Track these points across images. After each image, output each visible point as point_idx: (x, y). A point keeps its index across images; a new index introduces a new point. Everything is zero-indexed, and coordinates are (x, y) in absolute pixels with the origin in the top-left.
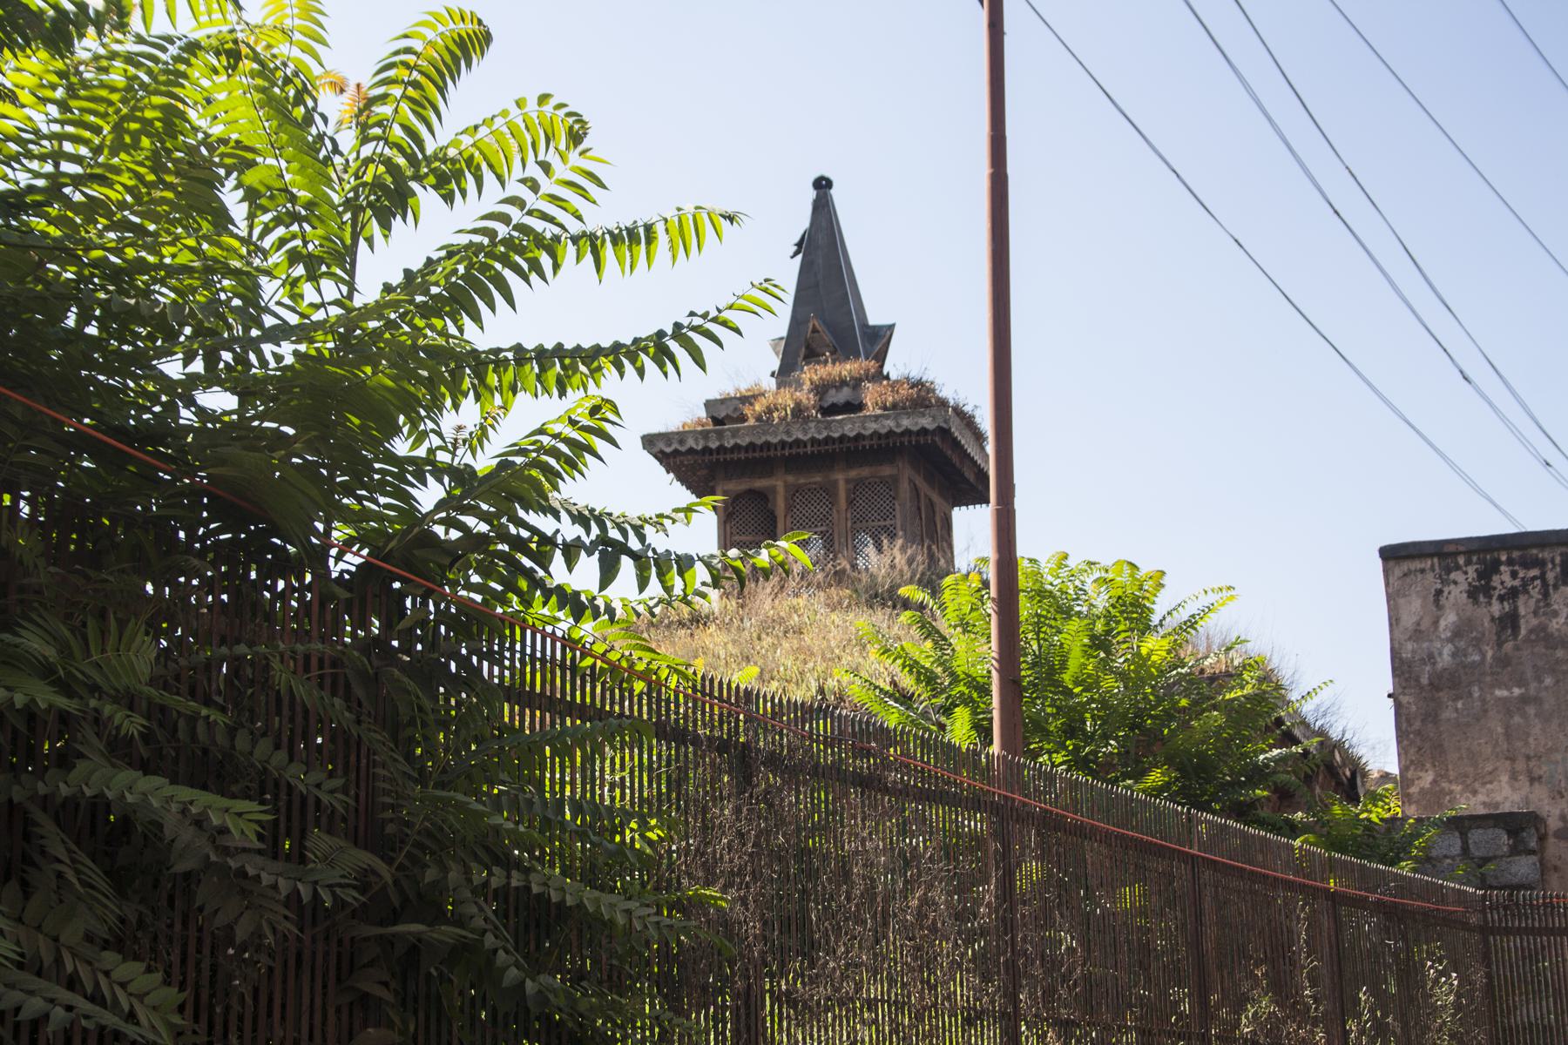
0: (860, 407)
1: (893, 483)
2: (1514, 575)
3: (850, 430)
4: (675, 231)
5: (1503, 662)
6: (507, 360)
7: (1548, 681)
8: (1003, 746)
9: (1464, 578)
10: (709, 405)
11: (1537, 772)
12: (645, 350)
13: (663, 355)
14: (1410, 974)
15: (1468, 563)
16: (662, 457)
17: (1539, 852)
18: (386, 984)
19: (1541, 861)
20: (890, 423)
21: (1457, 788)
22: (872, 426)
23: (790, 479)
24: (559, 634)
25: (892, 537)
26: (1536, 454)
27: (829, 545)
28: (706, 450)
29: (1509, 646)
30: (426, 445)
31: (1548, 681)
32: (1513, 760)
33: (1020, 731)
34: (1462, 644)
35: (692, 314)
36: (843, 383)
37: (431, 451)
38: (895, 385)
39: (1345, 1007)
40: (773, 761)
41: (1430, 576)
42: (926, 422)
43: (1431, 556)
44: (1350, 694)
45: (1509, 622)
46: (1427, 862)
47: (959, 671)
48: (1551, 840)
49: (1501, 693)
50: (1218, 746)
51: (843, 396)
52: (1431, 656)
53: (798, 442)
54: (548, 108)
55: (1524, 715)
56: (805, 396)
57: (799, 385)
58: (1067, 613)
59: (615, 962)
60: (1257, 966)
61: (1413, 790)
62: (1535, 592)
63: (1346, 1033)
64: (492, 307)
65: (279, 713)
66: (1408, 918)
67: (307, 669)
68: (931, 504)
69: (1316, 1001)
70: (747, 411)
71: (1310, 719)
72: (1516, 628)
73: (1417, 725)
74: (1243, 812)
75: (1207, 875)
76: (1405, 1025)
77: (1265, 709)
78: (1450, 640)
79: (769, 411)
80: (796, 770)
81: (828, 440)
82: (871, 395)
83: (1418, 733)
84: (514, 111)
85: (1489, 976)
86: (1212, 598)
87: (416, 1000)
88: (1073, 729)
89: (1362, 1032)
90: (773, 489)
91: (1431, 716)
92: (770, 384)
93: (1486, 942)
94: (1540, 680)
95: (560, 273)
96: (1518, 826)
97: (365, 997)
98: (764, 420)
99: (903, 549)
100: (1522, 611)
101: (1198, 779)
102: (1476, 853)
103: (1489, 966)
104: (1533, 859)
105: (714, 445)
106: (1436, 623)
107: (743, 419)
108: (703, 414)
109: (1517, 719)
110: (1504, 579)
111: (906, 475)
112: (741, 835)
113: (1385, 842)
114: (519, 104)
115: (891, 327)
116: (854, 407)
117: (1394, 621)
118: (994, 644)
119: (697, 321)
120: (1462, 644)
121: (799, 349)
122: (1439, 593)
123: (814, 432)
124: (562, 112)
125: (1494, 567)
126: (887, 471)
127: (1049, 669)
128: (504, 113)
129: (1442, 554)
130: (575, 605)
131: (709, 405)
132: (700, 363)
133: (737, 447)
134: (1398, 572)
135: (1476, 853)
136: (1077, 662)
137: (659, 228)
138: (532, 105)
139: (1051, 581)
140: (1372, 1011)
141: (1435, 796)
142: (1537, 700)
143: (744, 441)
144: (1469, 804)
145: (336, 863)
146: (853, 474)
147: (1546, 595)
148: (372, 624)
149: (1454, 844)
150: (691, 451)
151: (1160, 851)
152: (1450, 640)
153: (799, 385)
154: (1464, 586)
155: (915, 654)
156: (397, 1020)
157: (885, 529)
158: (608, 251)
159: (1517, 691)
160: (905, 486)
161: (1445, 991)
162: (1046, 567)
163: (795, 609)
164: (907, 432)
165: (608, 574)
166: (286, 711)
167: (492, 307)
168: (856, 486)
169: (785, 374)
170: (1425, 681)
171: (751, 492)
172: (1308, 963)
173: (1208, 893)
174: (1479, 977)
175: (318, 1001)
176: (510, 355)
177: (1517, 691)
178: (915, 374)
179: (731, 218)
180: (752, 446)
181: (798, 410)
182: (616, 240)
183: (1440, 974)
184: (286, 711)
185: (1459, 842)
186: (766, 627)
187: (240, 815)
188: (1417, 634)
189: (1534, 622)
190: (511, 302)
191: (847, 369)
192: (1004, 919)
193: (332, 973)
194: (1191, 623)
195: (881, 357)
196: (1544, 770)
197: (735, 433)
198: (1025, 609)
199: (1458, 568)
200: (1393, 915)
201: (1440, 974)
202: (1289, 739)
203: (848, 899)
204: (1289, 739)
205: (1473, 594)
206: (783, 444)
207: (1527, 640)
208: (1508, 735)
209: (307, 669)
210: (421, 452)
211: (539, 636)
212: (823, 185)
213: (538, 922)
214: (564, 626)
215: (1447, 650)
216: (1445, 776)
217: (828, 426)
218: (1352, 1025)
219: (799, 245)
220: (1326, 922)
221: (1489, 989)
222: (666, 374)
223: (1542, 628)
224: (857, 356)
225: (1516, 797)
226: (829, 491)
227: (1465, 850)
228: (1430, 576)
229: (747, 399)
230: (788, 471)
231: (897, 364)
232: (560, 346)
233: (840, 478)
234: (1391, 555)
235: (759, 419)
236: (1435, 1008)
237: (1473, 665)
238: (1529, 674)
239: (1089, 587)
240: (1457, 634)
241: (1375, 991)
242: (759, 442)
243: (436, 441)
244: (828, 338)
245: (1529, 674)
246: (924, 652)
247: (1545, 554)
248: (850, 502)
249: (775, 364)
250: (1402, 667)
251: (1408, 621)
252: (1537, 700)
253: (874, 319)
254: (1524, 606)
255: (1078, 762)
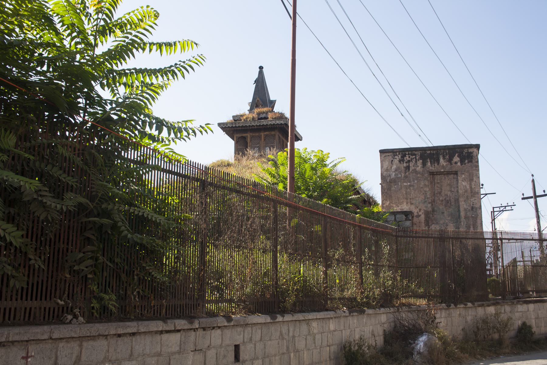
0: (267, 118)
1: (275, 135)
2: (409, 157)
3: (265, 123)
5: (406, 177)
6: (133, 72)
7: (416, 182)
8: (290, 190)
10: (233, 117)
11: (412, 202)
13: (174, 74)
15: (399, 154)
16: (222, 128)
18: (94, 235)
20: (274, 122)
21: (394, 205)
22: (270, 123)
23: (251, 134)
24: (152, 148)
25: (273, 148)
26: (418, 134)
27: (260, 151)
28: (232, 127)
29: (407, 173)
31: (416, 182)
32: (407, 199)
33: (294, 187)
34: (397, 173)
36: (264, 113)
37: (117, 99)
39: (362, 252)
40: (211, 184)
41: (390, 157)
42: (282, 122)
43: (391, 152)
44: (372, 185)
46: (386, 221)
47: (281, 174)
50: (343, 195)
52: (390, 175)
53: (253, 126)
54: (149, 9)
55: (410, 189)
56: (255, 115)
58: (305, 161)
62: (414, 161)
63: (361, 259)
64: (129, 57)
65: (65, 162)
66: (380, 234)
67: (75, 151)
68: (283, 141)
70: (242, 118)
71: (366, 191)
72: (409, 169)
73: (386, 191)
74: (346, 209)
76: (376, 258)
77: (353, 186)
78: (394, 172)
79: (247, 118)
81: (260, 125)
82: (270, 115)
84: (140, 9)
85: (397, 247)
86: (340, 160)
87: (104, 240)
88: (307, 189)
89: (365, 259)
90: (247, 136)
91: (389, 189)
93: (397, 239)
94: (414, 181)
97: (88, 239)
98: (246, 120)
101: (336, 201)
103: (397, 244)
105: (234, 126)
106: (391, 168)
107: (241, 120)
109: (408, 190)
110: (407, 158)
111: (277, 134)
114: (142, 8)
115: (275, 101)
116: (266, 118)
117: (382, 167)
118: (289, 168)
120: (397, 173)
121: (254, 105)
122: (392, 161)
123: (256, 123)
124: (153, 10)
125: (405, 155)
126: (273, 133)
127: (302, 175)
128: (137, 10)
130: (152, 138)
131: (233, 117)
134: (383, 156)
136: (308, 173)
138: (145, 8)
140: (368, 254)
141: (389, 207)
142: (413, 186)
144: (397, 209)
145: (71, 200)
147: (416, 162)
148: (95, 140)
149: (393, 218)
150: (229, 127)
151: (317, 214)
152: (394, 172)
156: (97, 245)
158: (164, 48)
159: (409, 184)
160: (277, 136)
161: (386, 250)
162: (301, 151)
163: (251, 163)
164: (278, 124)
165: (160, 130)
167: (129, 57)
168: (266, 136)
169: (251, 110)
170: (388, 181)
171: (242, 137)
172: (353, 242)
174: (395, 247)
175: (74, 239)
176: (134, 71)
177: (409, 184)
178: (280, 111)
181: (253, 118)
183: (385, 246)
185: (394, 218)
186: (244, 167)
187: (31, 183)
188: (387, 170)
189: (413, 168)
190: (134, 56)
191: (265, 109)
193: (79, 231)
195: (273, 107)
196: (414, 202)
197: (239, 123)
198: (297, 160)
199: (397, 155)
200: (374, 232)
201: (385, 246)
203: (232, 220)
204: (358, 193)
205: (400, 161)
206: (250, 126)
207: (411, 172)
208: (406, 194)
210: (115, 99)
211: (145, 148)
212: (261, 68)
214: (153, 146)
215: (394, 174)
216: (392, 203)
217: (260, 122)
218: (363, 257)
219: (255, 81)
220: (358, 233)
221: (397, 250)
223: (415, 169)
224: (267, 107)
225: (407, 208)
226: (260, 137)
227: (395, 219)
228: (390, 157)
229: (242, 116)
230: (251, 132)
231: (276, 109)
232: (146, 69)
233: (262, 134)
234: (382, 152)
236: (384, 254)
239: (312, 157)
240: (396, 170)
241: (370, 249)
242: (244, 125)
243: (118, 96)
244: (261, 103)
247: (417, 153)
248: (264, 140)
249: (249, 108)
250: (383, 177)
251: (385, 167)
254: (411, 164)
255: (310, 197)
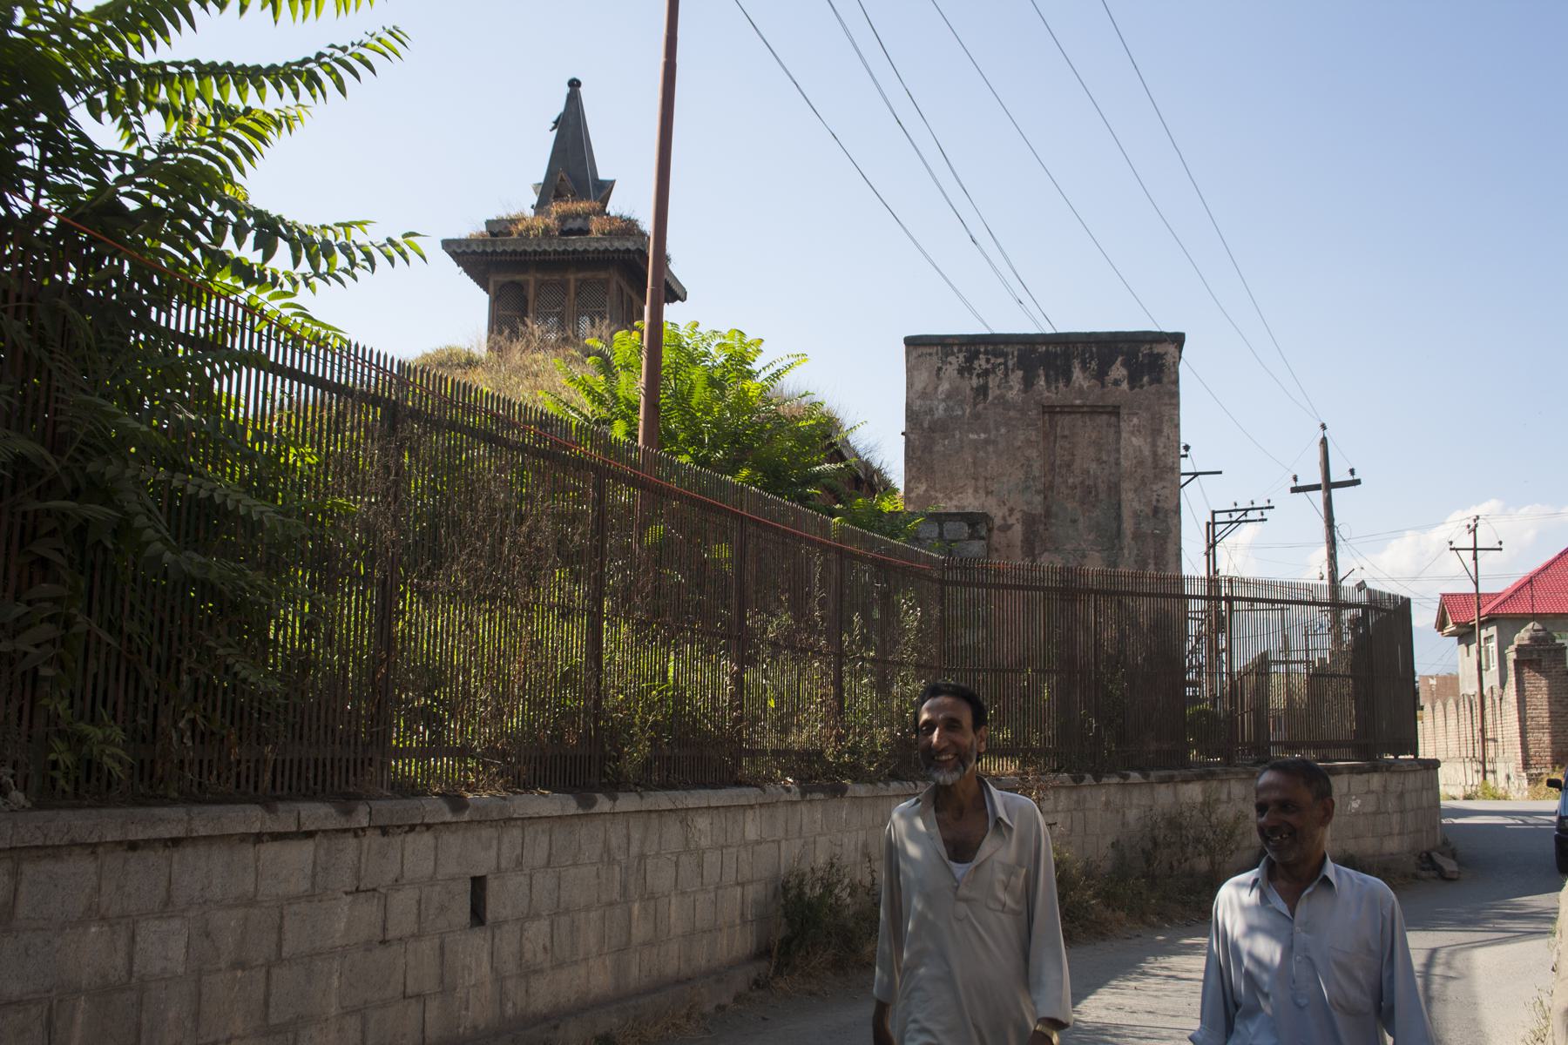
0: (588, 232)
2: (988, 361)
3: (580, 247)
5: (976, 416)
6: (189, 73)
8: (645, 442)
9: (957, 360)
10: (488, 223)
13: (313, 81)
14: (890, 609)
17: (988, 538)
18: (60, 551)
19: (988, 545)
20: (606, 244)
21: (940, 496)
22: (595, 245)
23: (539, 276)
24: (241, 301)
25: (602, 318)
26: (1014, 295)
28: (484, 253)
29: (980, 407)
30: (135, 145)
31: (1003, 431)
32: (976, 479)
35: (332, 46)
36: (578, 215)
37: (140, 150)
38: (611, 219)
39: (843, 624)
40: (415, 414)
42: (630, 245)
44: (879, 434)
45: (982, 391)
46: (915, 539)
47: (620, 394)
51: (577, 224)
52: (931, 410)
53: (545, 252)
56: (552, 221)
57: (549, 214)
61: (913, 495)
62: (1000, 373)
63: (841, 643)
66: (895, 573)
69: (823, 620)
70: (513, 229)
72: (986, 395)
73: (919, 453)
74: (804, 499)
75: (751, 529)
76: (883, 641)
77: (825, 436)
79: (528, 229)
82: (595, 224)
83: (919, 459)
85: (942, 611)
86: (792, 360)
88: (695, 440)
89: (852, 642)
90: (527, 282)
91: (928, 448)
92: (530, 213)
96: (975, 521)
98: (524, 235)
101: (774, 477)
102: (947, 536)
105: (489, 249)
106: (936, 388)
107: (510, 234)
108: (484, 229)
109: (981, 454)
110: (981, 363)
111: (615, 279)
113: (893, 524)
115: (613, 182)
116: (584, 232)
118: (643, 380)
119: (339, 54)
121: (550, 191)
122: (940, 369)
123: (556, 246)
125: (976, 356)
126: (602, 275)
127: (682, 399)
130: (245, 272)
131: (488, 223)
132: (341, 88)
133: (504, 252)
134: (915, 354)
135: (947, 536)
136: (700, 394)
139: (689, 342)
140: (861, 628)
141: (927, 499)
143: (509, 249)
146: (580, 275)
147: (1006, 375)
148: (69, 270)
149: (934, 530)
150: (474, 252)
153: (549, 214)
154: (956, 366)
157: (599, 313)
159: (983, 436)
160: (613, 286)
161: (912, 619)
162: (683, 331)
163: (536, 361)
164: (617, 250)
169: (540, 208)
170: (926, 425)
171: (512, 282)
174: (936, 612)
176: (192, 69)
177: (983, 436)
178: (626, 214)
181: (547, 231)
185: (937, 530)
186: (516, 370)
188: (924, 395)
191: (582, 206)
194: (777, 375)
195: (605, 201)
198: (668, 356)
200: (882, 568)
201: (910, 608)
204: (838, 456)
205: (961, 371)
206: (535, 252)
207: (992, 403)
208: (974, 463)
210: (133, 150)
211: (223, 302)
212: (574, 84)
213: (200, 520)
214: (245, 295)
215: (941, 407)
217: (566, 243)
219: (556, 123)
220: (834, 568)
221: (942, 620)
222: (314, 96)
223: (1002, 396)
224: (588, 198)
226: (564, 285)
227: (941, 534)
229: (514, 221)
231: (613, 208)
234: (911, 342)
235: (520, 234)
236: (904, 630)
238: (992, 425)
240: (949, 396)
241: (866, 616)
242: (519, 249)
243: (143, 142)
244: (570, 185)
245: (992, 425)
247: (1009, 349)
248: (577, 294)
249: (535, 200)
250: (912, 415)
251: (919, 386)
252: (995, 443)
253: (602, 176)
254: (992, 382)
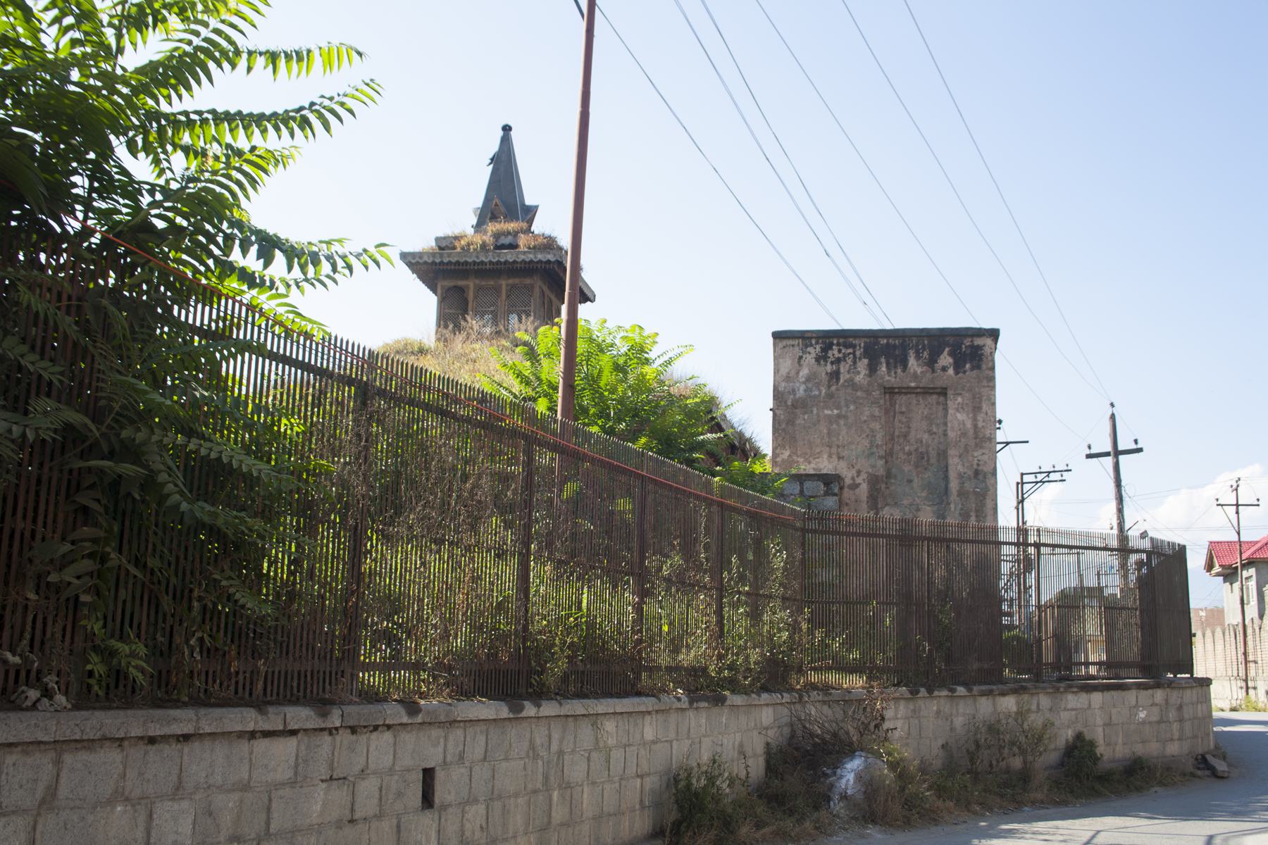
1: (530, 288)
2: (840, 351)
3: (510, 258)
4: (325, 56)
5: (830, 396)
6: (207, 119)
9: (815, 350)
10: (437, 239)
11: (842, 454)
12: (294, 119)
13: (305, 123)
16: (411, 265)
17: (839, 495)
18: (99, 501)
20: (531, 256)
21: (801, 460)
22: (522, 257)
23: (477, 282)
24: (245, 301)
25: (528, 315)
27: (495, 321)
29: (834, 388)
30: (164, 177)
31: (852, 407)
32: (830, 447)
35: (323, 97)
36: (509, 233)
37: (167, 181)
38: (536, 237)
42: (551, 257)
44: (752, 412)
46: (781, 495)
47: (543, 376)
48: (846, 490)
49: (827, 412)
50: (687, 433)
52: (794, 391)
53: (482, 262)
55: (838, 425)
56: (488, 238)
59: (267, 502)
60: (675, 539)
62: (849, 361)
65: (36, 325)
68: (551, 301)
70: (457, 244)
72: (838, 379)
73: (783, 426)
74: (690, 462)
75: (650, 487)
76: (756, 578)
77: (707, 412)
79: (469, 245)
80: (396, 400)
81: (498, 262)
82: (523, 240)
83: (784, 430)
85: (803, 554)
86: (682, 350)
87: (124, 514)
88: (603, 414)
90: (468, 287)
91: (791, 422)
92: (470, 231)
95: (252, 72)
96: (829, 480)
98: (466, 249)
99: (533, 322)
100: (842, 370)
101: (667, 444)
104: (836, 498)
105: (438, 260)
106: (798, 373)
107: (454, 248)
108: (433, 244)
110: (834, 353)
111: (538, 284)
112: (359, 435)
113: (763, 482)
116: (513, 246)
117: (777, 371)
118: (562, 365)
119: (327, 103)
121: (488, 213)
122: (801, 358)
123: (491, 257)
125: (830, 347)
126: (528, 281)
127: (593, 381)
129: (804, 338)
130: (248, 278)
131: (437, 239)
133: (450, 263)
134: (781, 345)
136: (607, 378)
137: (316, 53)
139: (599, 335)
140: (738, 568)
141: (789, 463)
143: (454, 260)
144: (806, 468)
146: (510, 281)
150: (426, 263)
153: (486, 232)
154: (814, 355)
155: (520, 367)
158: (282, 62)
159: (836, 412)
160: (537, 290)
161: (779, 561)
164: (540, 261)
166: (41, 325)
168: (512, 288)
169: (479, 226)
170: (789, 403)
173: (650, 498)
174: (798, 555)
177: (836, 412)
178: (547, 233)
179: (360, 54)
180: (458, 263)
181: (484, 246)
182: (288, 57)
184: (41, 325)
186: (458, 357)
188: (788, 378)
190: (211, 81)
191: (512, 226)
192: (525, 501)
195: (530, 222)
196: (845, 453)
197: (449, 255)
198: (581, 346)
200: (755, 518)
201: (777, 551)
202: (718, 428)
203: (427, 479)
204: (718, 428)
205: (818, 360)
206: (474, 263)
207: (843, 385)
208: (829, 434)
209: (59, 299)
210: (161, 182)
212: (507, 129)
215: (802, 388)
216: (795, 453)
220: (717, 519)
221: (803, 561)
223: (851, 380)
224: (517, 219)
226: (497, 290)
227: (802, 492)
228: (797, 349)
229: (457, 238)
231: (539, 226)
233: (504, 283)
234: (778, 336)
235: (463, 248)
237: (815, 396)
238: (843, 403)
240: (808, 380)
241: (742, 558)
242: (462, 260)
244: (503, 209)
245: (843, 403)
246: (526, 367)
247: (856, 342)
248: (508, 296)
249: (474, 221)
250: (778, 395)
251: (784, 371)
252: (845, 417)
254: (843, 368)
